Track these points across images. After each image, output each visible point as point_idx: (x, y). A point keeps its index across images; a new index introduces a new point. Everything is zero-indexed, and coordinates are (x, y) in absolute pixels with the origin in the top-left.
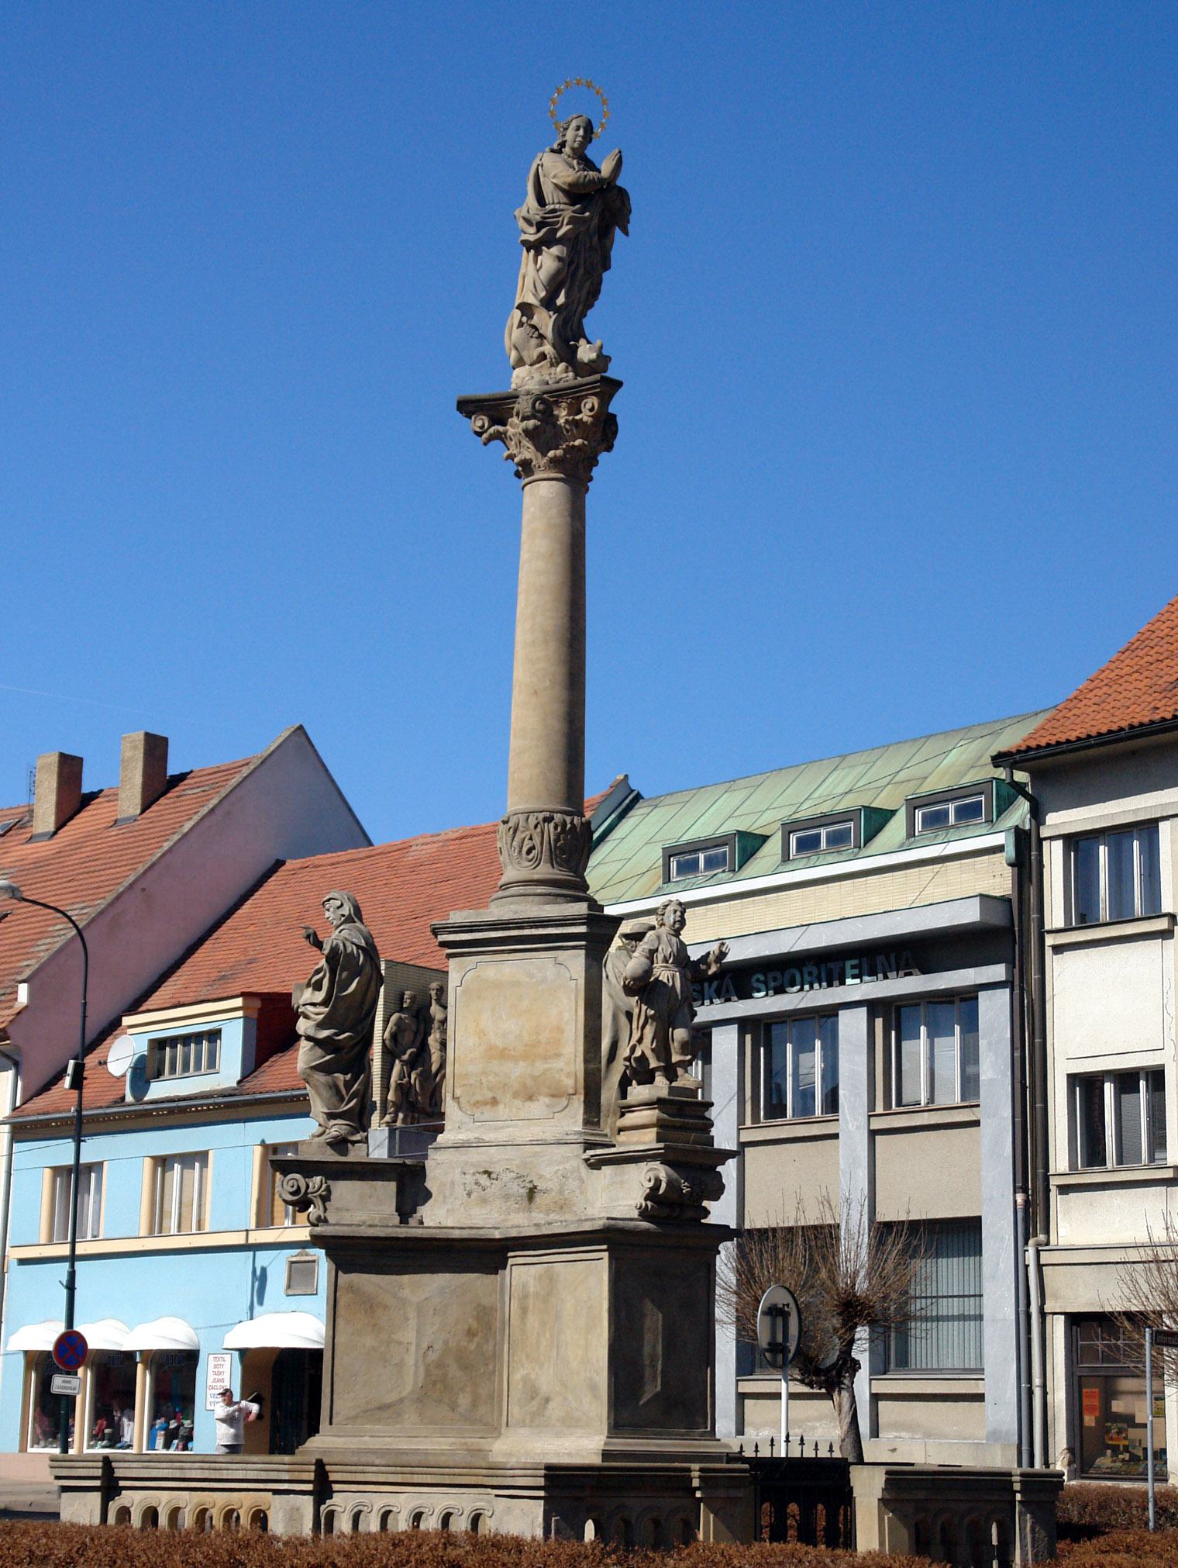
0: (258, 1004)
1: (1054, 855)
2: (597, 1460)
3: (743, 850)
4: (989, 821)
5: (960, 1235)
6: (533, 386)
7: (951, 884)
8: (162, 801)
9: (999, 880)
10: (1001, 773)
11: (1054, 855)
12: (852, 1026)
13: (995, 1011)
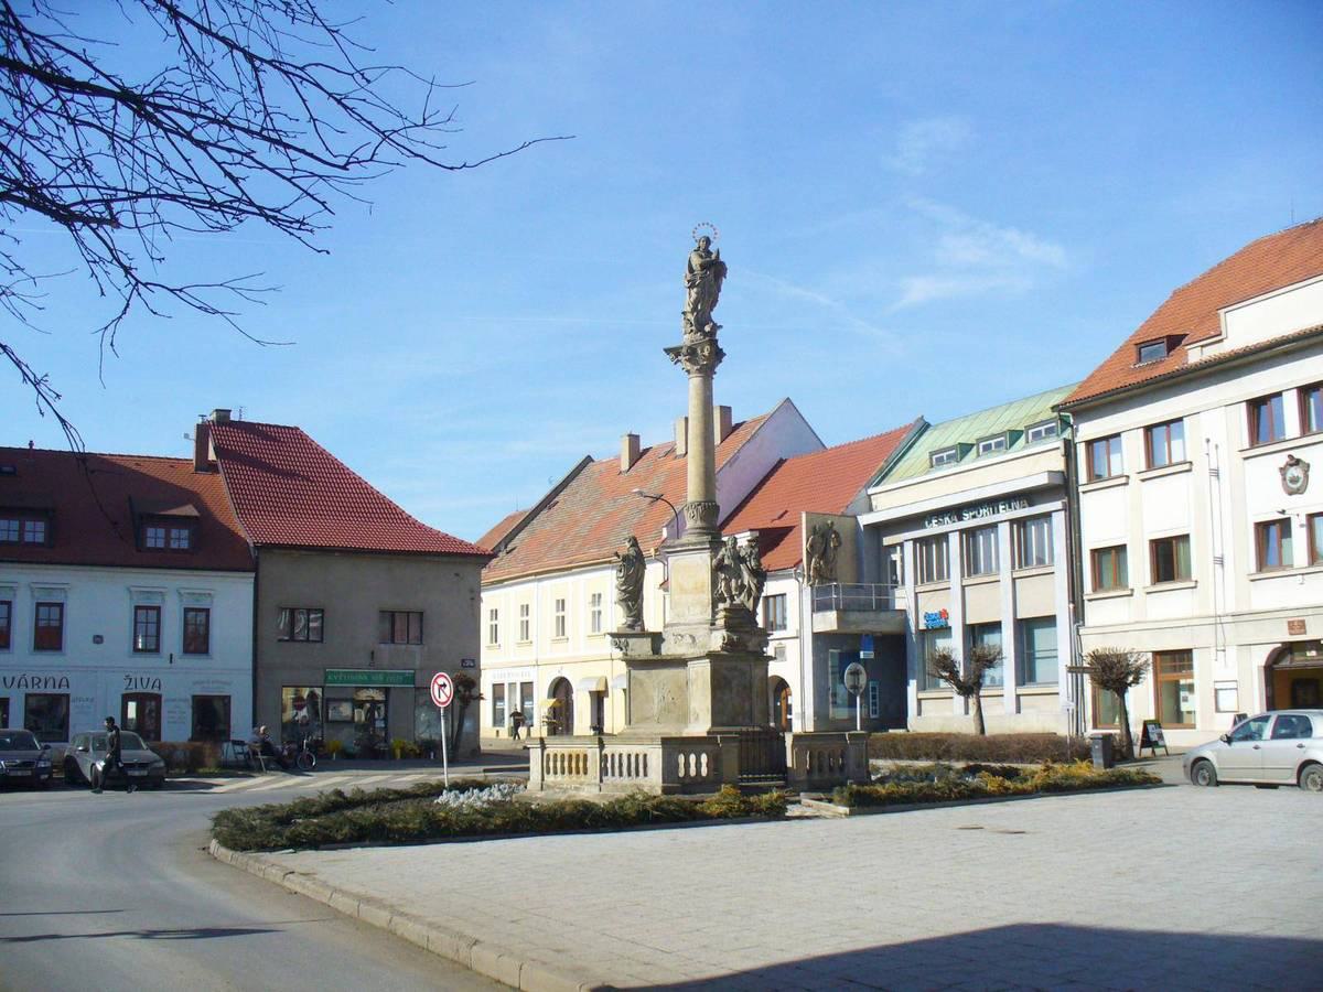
0: (757, 534)
1: (1081, 450)
2: (705, 735)
3: (961, 450)
4: (1058, 435)
5: (1050, 621)
6: (688, 344)
7: (1036, 465)
8: (731, 437)
9: (1058, 463)
10: (1056, 414)
11: (1081, 450)
12: (954, 539)
13: (1059, 520)
